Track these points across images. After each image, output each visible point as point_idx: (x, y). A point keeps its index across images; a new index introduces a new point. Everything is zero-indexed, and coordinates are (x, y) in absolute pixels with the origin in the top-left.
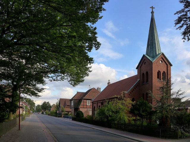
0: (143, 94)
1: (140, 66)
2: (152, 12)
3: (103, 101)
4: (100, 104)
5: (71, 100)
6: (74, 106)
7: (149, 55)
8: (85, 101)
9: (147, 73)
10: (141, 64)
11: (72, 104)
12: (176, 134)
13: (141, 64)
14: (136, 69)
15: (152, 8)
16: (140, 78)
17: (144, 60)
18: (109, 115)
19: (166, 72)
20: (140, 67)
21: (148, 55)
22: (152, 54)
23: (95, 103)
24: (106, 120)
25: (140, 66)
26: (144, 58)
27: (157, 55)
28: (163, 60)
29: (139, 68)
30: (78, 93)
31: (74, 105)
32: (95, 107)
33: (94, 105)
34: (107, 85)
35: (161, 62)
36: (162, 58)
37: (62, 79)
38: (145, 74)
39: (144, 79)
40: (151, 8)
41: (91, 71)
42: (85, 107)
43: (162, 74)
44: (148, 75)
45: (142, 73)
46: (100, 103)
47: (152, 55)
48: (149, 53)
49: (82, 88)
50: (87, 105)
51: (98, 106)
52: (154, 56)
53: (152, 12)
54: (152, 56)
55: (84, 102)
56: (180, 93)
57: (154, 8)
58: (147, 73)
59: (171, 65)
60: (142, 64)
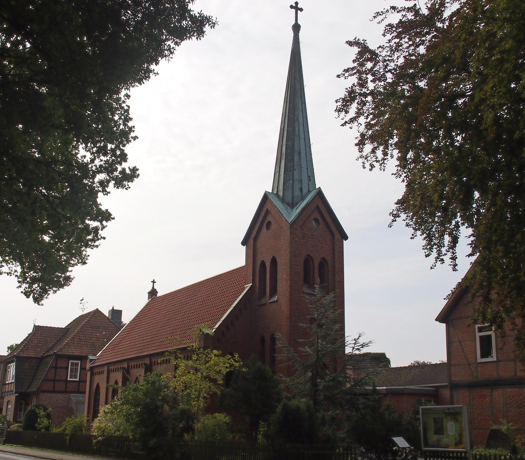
0: (263, 340)
1: (253, 236)
2: (296, 28)
3: (132, 364)
4: (118, 376)
9: (274, 261)
10: (258, 225)
12: (294, 70)
13: (258, 225)
14: (440, 319)
15: (296, 8)
16: (253, 282)
17: (267, 212)
19: (329, 259)
23: (102, 373)
26: (268, 206)
28: (319, 218)
29: (251, 241)
30: (37, 328)
32: (98, 387)
33: (97, 379)
34: (144, 300)
35: (314, 223)
36: (318, 208)
40: (292, 7)
43: (316, 264)
45: (258, 264)
46: (117, 370)
49: (60, 309)
50: (66, 381)
51: (112, 382)
53: (296, 28)
54: (290, 201)
56: (361, 341)
57: (301, 10)
59: (346, 238)
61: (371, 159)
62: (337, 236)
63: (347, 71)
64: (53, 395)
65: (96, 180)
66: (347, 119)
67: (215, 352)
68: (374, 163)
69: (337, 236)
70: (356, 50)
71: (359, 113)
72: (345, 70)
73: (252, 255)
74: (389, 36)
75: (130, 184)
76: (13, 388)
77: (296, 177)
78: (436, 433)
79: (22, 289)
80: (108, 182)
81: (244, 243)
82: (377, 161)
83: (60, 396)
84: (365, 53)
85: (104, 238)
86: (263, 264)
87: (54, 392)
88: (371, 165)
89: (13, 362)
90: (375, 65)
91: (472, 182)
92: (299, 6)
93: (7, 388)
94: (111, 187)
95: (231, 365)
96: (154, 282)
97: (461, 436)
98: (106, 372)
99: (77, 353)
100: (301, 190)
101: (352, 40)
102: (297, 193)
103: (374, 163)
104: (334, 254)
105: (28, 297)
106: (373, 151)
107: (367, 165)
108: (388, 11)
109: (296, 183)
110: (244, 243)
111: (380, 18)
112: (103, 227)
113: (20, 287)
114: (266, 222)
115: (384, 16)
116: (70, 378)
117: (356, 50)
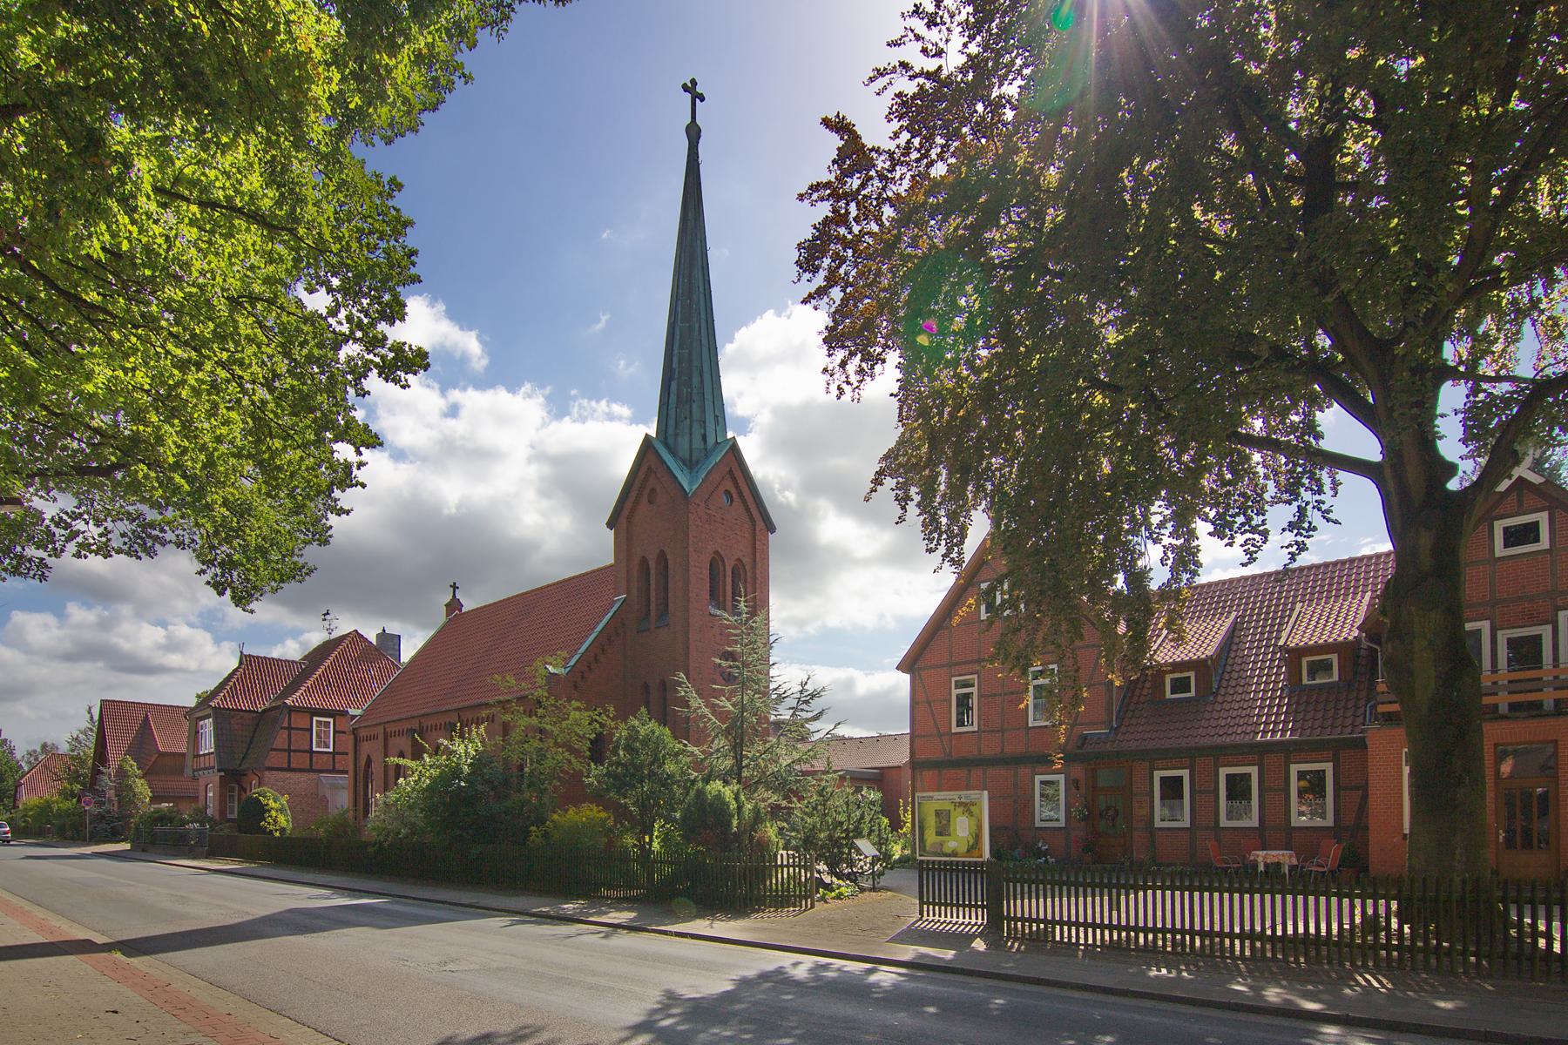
1: (626, 512)
2: (694, 133)
5: (192, 715)
6: (220, 762)
7: (671, 441)
8: (299, 721)
9: (662, 558)
11: (208, 745)
13: (633, 494)
18: (148, 249)
20: (629, 519)
21: (667, 445)
22: (687, 438)
23: (375, 737)
24: (1450, 352)
25: (626, 512)
27: (707, 454)
28: (733, 491)
29: (623, 520)
31: (217, 746)
32: (369, 762)
37: (143, 543)
38: (652, 564)
39: (648, 599)
41: (348, 512)
42: (300, 760)
44: (666, 577)
46: (401, 733)
47: (687, 446)
48: (671, 431)
50: (311, 752)
52: (695, 454)
53: (694, 133)
54: (687, 456)
55: (290, 728)
56: (810, 687)
58: (662, 558)
59: (771, 528)
60: (636, 502)
61: (839, 377)
62: (760, 524)
63: (815, 188)
64: (288, 775)
65: (342, 355)
66: (812, 288)
67: (575, 704)
68: (844, 386)
69: (760, 524)
70: (835, 141)
71: (832, 280)
72: (811, 188)
73: (624, 544)
74: (895, 125)
75: (410, 377)
76: (213, 761)
77: (696, 414)
78: (939, 833)
79: (207, 577)
80: (368, 366)
81: (610, 525)
82: (848, 383)
83: (303, 777)
84: (854, 155)
85: (364, 486)
86: (644, 561)
87: (289, 769)
88: (839, 388)
89: (208, 717)
90: (863, 186)
91: (1412, 243)
92: (699, 89)
93: (203, 762)
94: (373, 382)
95: (602, 726)
96: (454, 587)
97: (978, 837)
98: (381, 738)
99: (327, 705)
100: (704, 437)
101: (832, 116)
102: (698, 443)
103: (844, 386)
104: (754, 554)
105: (221, 593)
106: (843, 364)
107: (833, 388)
108: (894, 71)
109: (696, 426)
110: (610, 525)
111: (882, 82)
112: (361, 465)
113: (202, 572)
114: (647, 491)
115: (886, 79)
116: (1229, 818)
117: (835, 141)
